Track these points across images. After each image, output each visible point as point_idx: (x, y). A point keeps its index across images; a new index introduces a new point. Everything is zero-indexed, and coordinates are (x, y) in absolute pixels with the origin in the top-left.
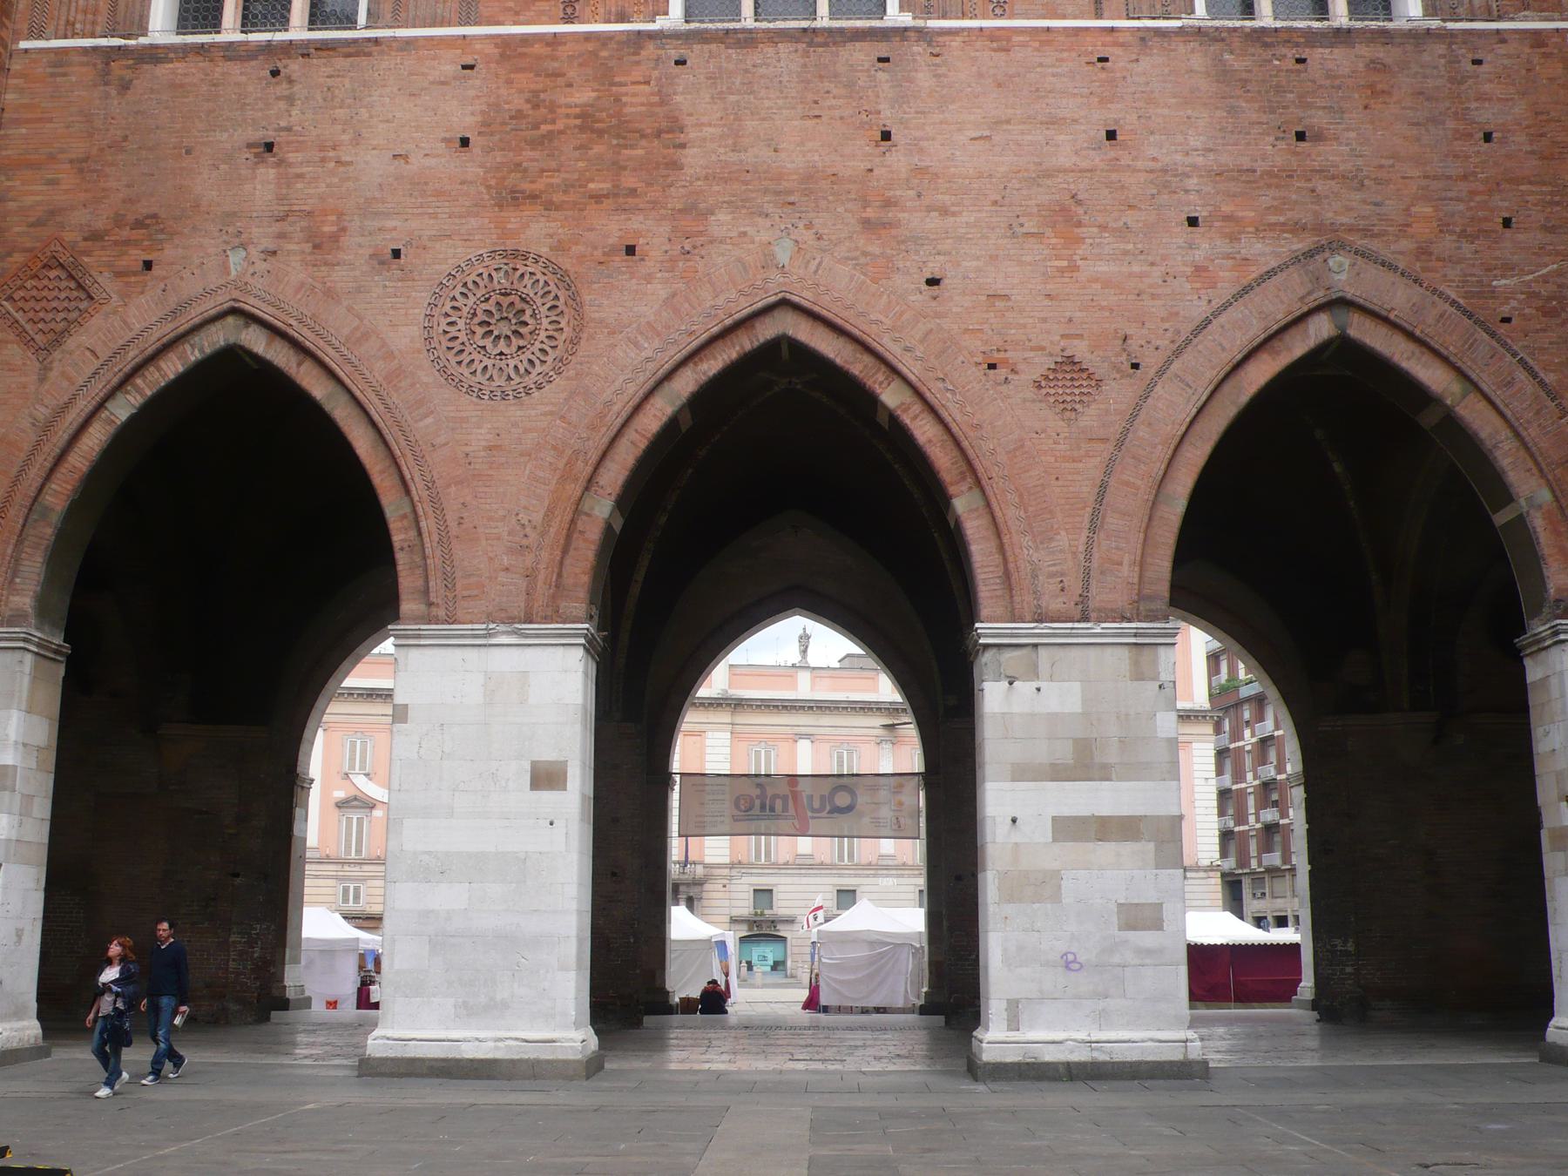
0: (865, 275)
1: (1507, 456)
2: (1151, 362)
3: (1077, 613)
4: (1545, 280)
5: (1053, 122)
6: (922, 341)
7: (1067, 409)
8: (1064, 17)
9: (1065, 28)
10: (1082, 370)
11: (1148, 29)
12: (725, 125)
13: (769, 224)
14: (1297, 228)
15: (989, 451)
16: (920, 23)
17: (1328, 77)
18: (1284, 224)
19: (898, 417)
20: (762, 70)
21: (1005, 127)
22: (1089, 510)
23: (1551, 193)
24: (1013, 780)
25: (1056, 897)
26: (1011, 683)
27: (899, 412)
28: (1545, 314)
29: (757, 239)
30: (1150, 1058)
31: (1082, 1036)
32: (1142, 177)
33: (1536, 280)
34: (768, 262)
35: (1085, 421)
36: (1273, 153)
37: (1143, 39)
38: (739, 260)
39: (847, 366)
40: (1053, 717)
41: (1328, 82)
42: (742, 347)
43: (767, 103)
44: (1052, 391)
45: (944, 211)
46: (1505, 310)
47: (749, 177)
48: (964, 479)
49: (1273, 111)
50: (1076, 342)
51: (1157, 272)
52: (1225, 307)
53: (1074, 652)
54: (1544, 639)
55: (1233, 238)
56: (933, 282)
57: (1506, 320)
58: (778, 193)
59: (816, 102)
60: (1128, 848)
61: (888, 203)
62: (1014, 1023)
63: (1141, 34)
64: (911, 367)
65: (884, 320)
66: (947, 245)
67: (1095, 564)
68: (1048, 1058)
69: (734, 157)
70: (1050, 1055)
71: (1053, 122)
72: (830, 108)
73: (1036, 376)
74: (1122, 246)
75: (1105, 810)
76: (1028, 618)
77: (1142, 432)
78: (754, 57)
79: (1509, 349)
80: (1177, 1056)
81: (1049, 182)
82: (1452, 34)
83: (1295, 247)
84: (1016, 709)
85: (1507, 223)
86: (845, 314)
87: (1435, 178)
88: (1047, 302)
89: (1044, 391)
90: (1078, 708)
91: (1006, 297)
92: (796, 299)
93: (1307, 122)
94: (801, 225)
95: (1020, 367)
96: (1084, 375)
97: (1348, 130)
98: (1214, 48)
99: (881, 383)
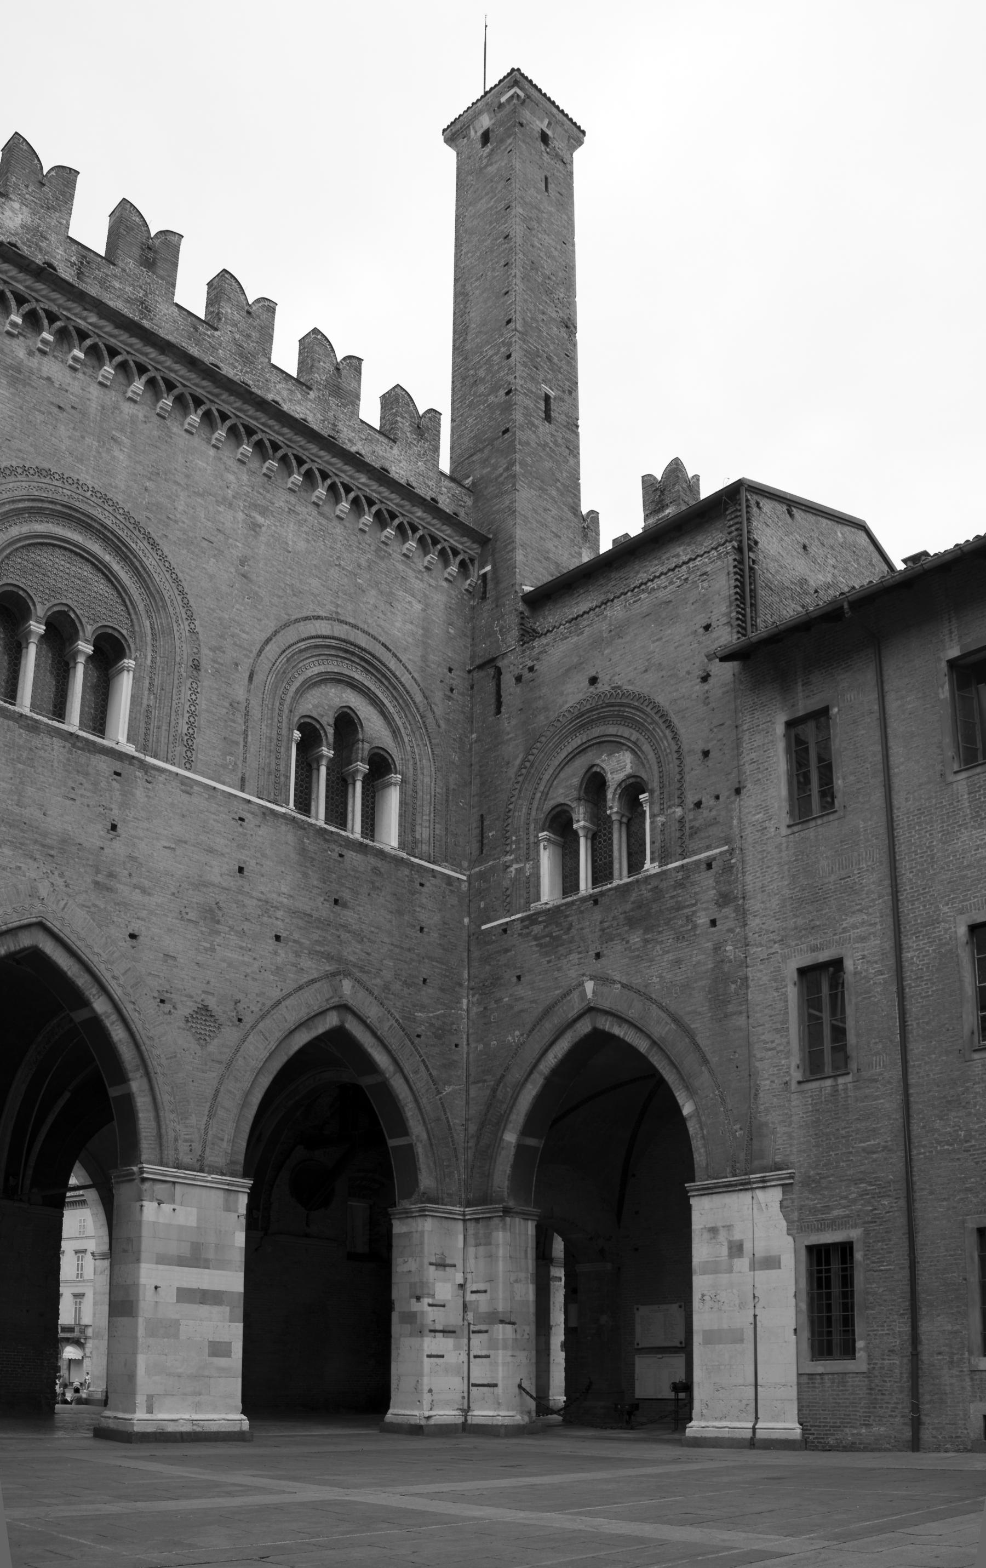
0: (94, 920)
1: (410, 1111)
2: (249, 1020)
3: (197, 1166)
4: (437, 1017)
5: (210, 851)
6: (123, 974)
7: (203, 1040)
8: (224, 783)
9: (224, 791)
10: (211, 1016)
11: (267, 808)
12: (13, 784)
13: (36, 865)
14: (329, 957)
15: (158, 1055)
16: (141, 756)
17: (353, 870)
18: (323, 953)
19: (102, 1021)
20: (41, 753)
21: (184, 845)
22: (209, 1104)
23: (446, 970)
24: (157, 1263)
25: (176, 1336)
26: (159, 1204)
27: (103, 1017)
28: (436, 1037)
29: (27, 874)
30: (223, 1430)
31: (187, 1416)
32: (255, 902)
33: (433, 1017)
34: (33, 894)
35: (212, 1048)
36: (324, 909)
37: (264, 814)
38: (15, 886)
39: (74, 979)
40: (181, 1228)
41: (352, 873)
42: (8, 947)
43: (42, 778)
44: (194, 1025)
45: (144, 891)
46: (419, 1031)
47: (26, 827)
48: (138, 1070)
49: (325, 883)
50: (210, 997)
51: (256, 965)
52: (290, 995)
53: (198, 1190)
54: (412, 1212)
55: (297, 955)
56: (133, 936)
57: (419, 1036)
58: (43, 846)
59: (73, 789)
60: (216, 1309)
61: (111, 875)
62: (150, 1410)
63: (264, 810)
64: (117, 991)
65: (102, 954)
66: (144, 914)
67: (210, 1137)
68: (170, 1429)
69: (17, 810)
70: (170, 1428)
71: (210, 851)
72: (82, 796)
73: (187, 1014)
74: (240, 943)
75: (205, 1286)
76: (171, 1165)
77: (240, 1062)
78: (37, 741)
79: (419, 1053)
80: (237, 1429)
81: (205, 890)
82: (413, 865)
83: (328, 968)
84: (161, 1220)
85: (425, 981)
86: (79, 943)
87: (396, 946)
88: (196, 967)
89: (190, 1024)
90: (194, 1224)
91: (174, 958)
92: (49, 924)
93: (340, 894)
94: (56, 873)
95: (179, 1006)
96: (212, 1019)
97: (359, 905)
98: (300, 832)
99: (94, 995)
